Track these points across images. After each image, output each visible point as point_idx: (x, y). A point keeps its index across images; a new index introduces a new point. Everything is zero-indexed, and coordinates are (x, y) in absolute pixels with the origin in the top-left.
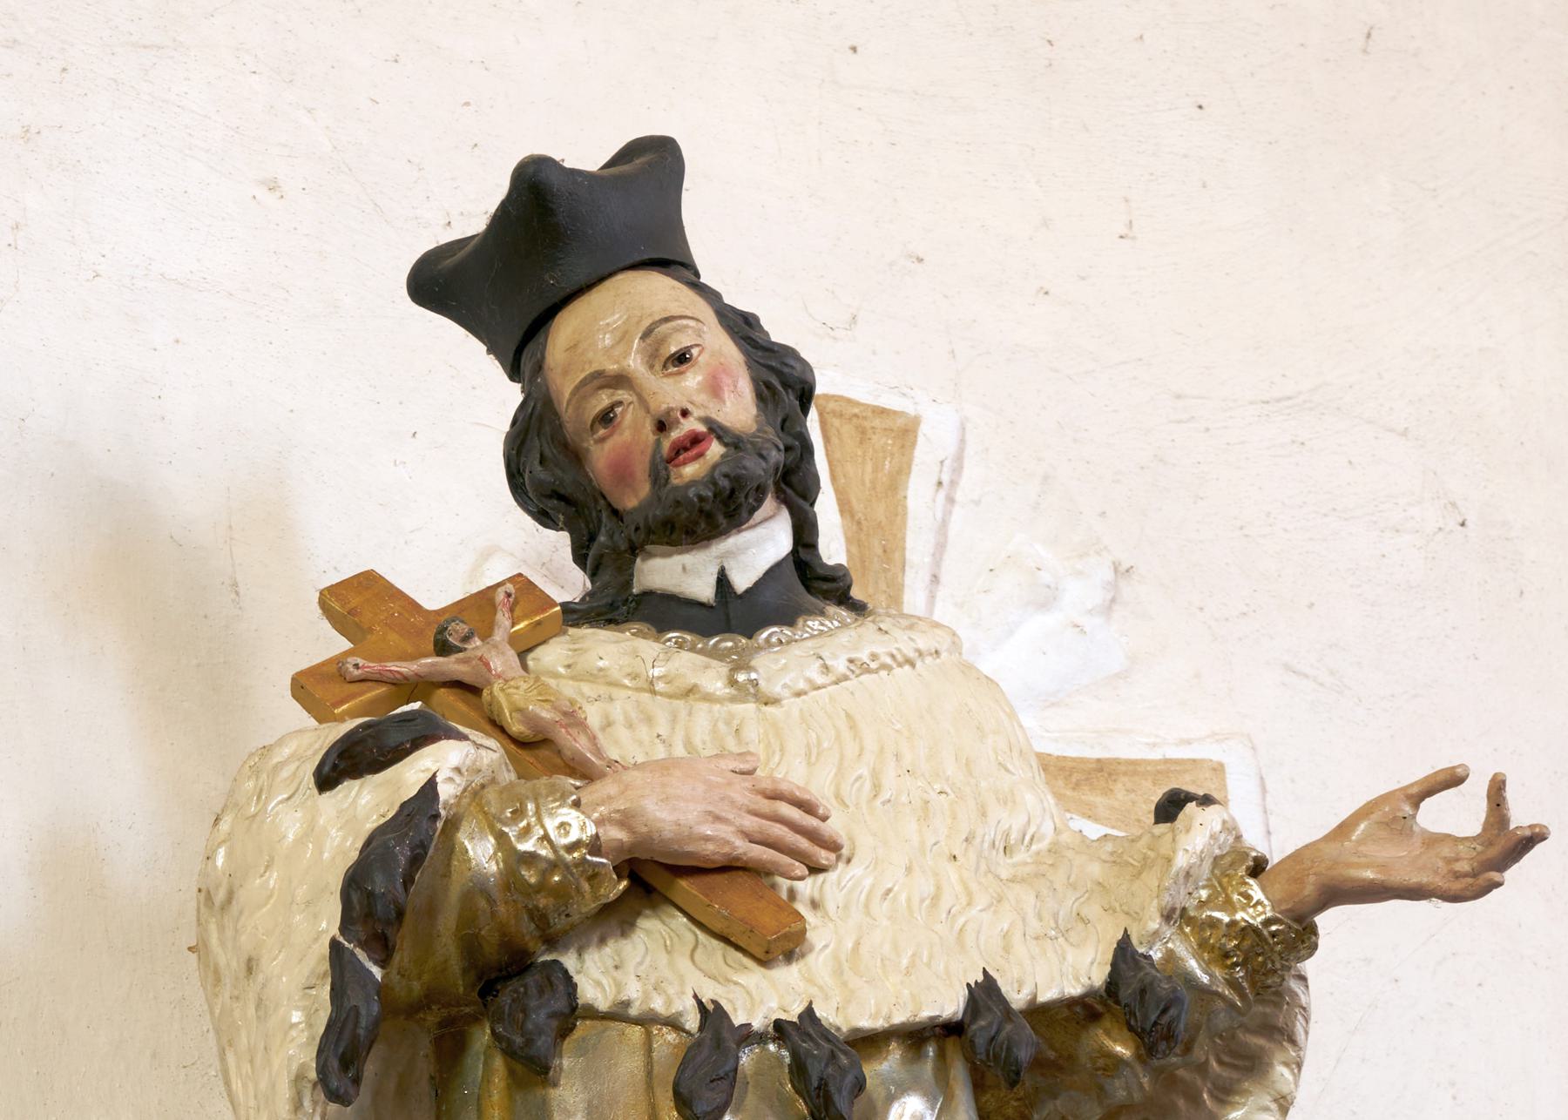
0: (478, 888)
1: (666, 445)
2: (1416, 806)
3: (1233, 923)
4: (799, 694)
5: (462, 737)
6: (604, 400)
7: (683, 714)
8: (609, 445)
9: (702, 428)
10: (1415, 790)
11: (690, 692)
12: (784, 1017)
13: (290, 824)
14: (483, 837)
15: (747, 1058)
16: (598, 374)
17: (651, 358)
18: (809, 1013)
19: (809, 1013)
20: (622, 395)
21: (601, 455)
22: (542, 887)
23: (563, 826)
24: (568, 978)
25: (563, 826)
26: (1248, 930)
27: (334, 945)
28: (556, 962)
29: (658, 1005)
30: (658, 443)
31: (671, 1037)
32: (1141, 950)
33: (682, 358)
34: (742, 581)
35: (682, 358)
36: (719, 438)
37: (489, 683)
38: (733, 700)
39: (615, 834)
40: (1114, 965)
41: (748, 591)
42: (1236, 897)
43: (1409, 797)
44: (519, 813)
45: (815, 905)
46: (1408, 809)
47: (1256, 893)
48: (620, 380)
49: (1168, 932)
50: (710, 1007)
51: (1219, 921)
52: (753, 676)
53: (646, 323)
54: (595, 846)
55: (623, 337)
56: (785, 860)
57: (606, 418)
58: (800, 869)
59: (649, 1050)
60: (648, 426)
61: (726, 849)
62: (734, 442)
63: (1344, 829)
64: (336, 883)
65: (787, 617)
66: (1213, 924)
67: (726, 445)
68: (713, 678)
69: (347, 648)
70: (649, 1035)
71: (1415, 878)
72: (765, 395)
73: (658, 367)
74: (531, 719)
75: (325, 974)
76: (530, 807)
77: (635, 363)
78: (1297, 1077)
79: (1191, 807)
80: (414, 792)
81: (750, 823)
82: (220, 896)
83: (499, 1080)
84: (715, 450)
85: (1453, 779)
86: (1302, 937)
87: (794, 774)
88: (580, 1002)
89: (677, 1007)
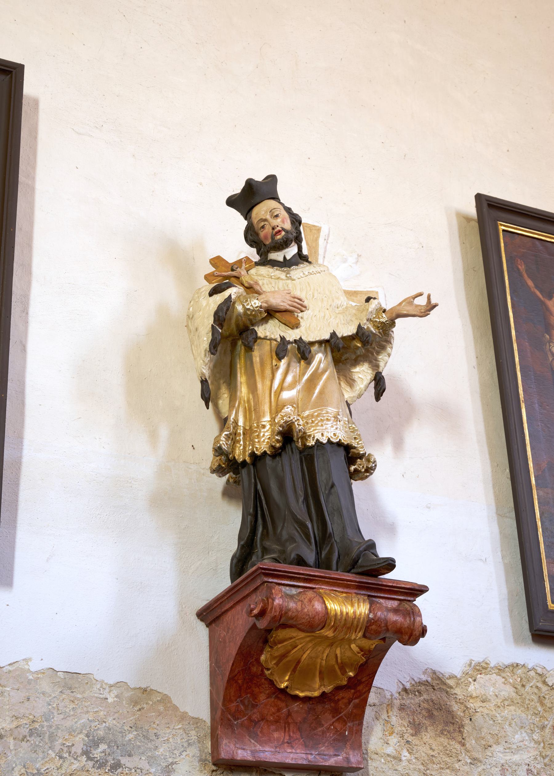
0: (239, 315)
1: (274, 232)
2: (414, 299)
3: (380, 321)
5: (236, 287)
6: (262, 224)
7: (277, 282)
9: (281, 229)
10: (414, 297)
12: (296, 339)
13: (204, 303)
14: (240, 305)
15: (289, 347)
17: (271, 216)
18: (301, 338)
19: (301, 338)
20: (266, 223)
21: (262, 234)
22: (251, 315)
27: (212, 325)
29: (273, 337)
31: (275, 342)
33: (277, 216)
34: (288, 258)
35: (277, 216)
36: (284, 231)
39: (265, 305)
42: (380, 316)
43: (413, 298)
44: (247, 301)
45: (302, 318)
46: (412, 300)
48: (266, 220)
50: (282, 337)
52: (290, 275)
54: (261, 307)
55: (266, 212)
56: (296, 309)
57: (263, 227)
58: (299, 311)
59: (271, 345)
60: (271, 229)
61: (285, 308)
62: (287, 232)
63: (400, 304)
64: (213, 314)
66: (376, 321)
67: (285, 232)
68: (283, 276)
70: (271, 342)
71: (414, 313)
72: (293, 223)
73: (273, 218)
76: (249, 300)
77: (268, 217)
78: (392, 350)
79: (372, 300)
81: (290, 303)
82: (191, 316)
84: (283, 233)
87: (298, 294)
88: (258, 336)
89: (276, 337)
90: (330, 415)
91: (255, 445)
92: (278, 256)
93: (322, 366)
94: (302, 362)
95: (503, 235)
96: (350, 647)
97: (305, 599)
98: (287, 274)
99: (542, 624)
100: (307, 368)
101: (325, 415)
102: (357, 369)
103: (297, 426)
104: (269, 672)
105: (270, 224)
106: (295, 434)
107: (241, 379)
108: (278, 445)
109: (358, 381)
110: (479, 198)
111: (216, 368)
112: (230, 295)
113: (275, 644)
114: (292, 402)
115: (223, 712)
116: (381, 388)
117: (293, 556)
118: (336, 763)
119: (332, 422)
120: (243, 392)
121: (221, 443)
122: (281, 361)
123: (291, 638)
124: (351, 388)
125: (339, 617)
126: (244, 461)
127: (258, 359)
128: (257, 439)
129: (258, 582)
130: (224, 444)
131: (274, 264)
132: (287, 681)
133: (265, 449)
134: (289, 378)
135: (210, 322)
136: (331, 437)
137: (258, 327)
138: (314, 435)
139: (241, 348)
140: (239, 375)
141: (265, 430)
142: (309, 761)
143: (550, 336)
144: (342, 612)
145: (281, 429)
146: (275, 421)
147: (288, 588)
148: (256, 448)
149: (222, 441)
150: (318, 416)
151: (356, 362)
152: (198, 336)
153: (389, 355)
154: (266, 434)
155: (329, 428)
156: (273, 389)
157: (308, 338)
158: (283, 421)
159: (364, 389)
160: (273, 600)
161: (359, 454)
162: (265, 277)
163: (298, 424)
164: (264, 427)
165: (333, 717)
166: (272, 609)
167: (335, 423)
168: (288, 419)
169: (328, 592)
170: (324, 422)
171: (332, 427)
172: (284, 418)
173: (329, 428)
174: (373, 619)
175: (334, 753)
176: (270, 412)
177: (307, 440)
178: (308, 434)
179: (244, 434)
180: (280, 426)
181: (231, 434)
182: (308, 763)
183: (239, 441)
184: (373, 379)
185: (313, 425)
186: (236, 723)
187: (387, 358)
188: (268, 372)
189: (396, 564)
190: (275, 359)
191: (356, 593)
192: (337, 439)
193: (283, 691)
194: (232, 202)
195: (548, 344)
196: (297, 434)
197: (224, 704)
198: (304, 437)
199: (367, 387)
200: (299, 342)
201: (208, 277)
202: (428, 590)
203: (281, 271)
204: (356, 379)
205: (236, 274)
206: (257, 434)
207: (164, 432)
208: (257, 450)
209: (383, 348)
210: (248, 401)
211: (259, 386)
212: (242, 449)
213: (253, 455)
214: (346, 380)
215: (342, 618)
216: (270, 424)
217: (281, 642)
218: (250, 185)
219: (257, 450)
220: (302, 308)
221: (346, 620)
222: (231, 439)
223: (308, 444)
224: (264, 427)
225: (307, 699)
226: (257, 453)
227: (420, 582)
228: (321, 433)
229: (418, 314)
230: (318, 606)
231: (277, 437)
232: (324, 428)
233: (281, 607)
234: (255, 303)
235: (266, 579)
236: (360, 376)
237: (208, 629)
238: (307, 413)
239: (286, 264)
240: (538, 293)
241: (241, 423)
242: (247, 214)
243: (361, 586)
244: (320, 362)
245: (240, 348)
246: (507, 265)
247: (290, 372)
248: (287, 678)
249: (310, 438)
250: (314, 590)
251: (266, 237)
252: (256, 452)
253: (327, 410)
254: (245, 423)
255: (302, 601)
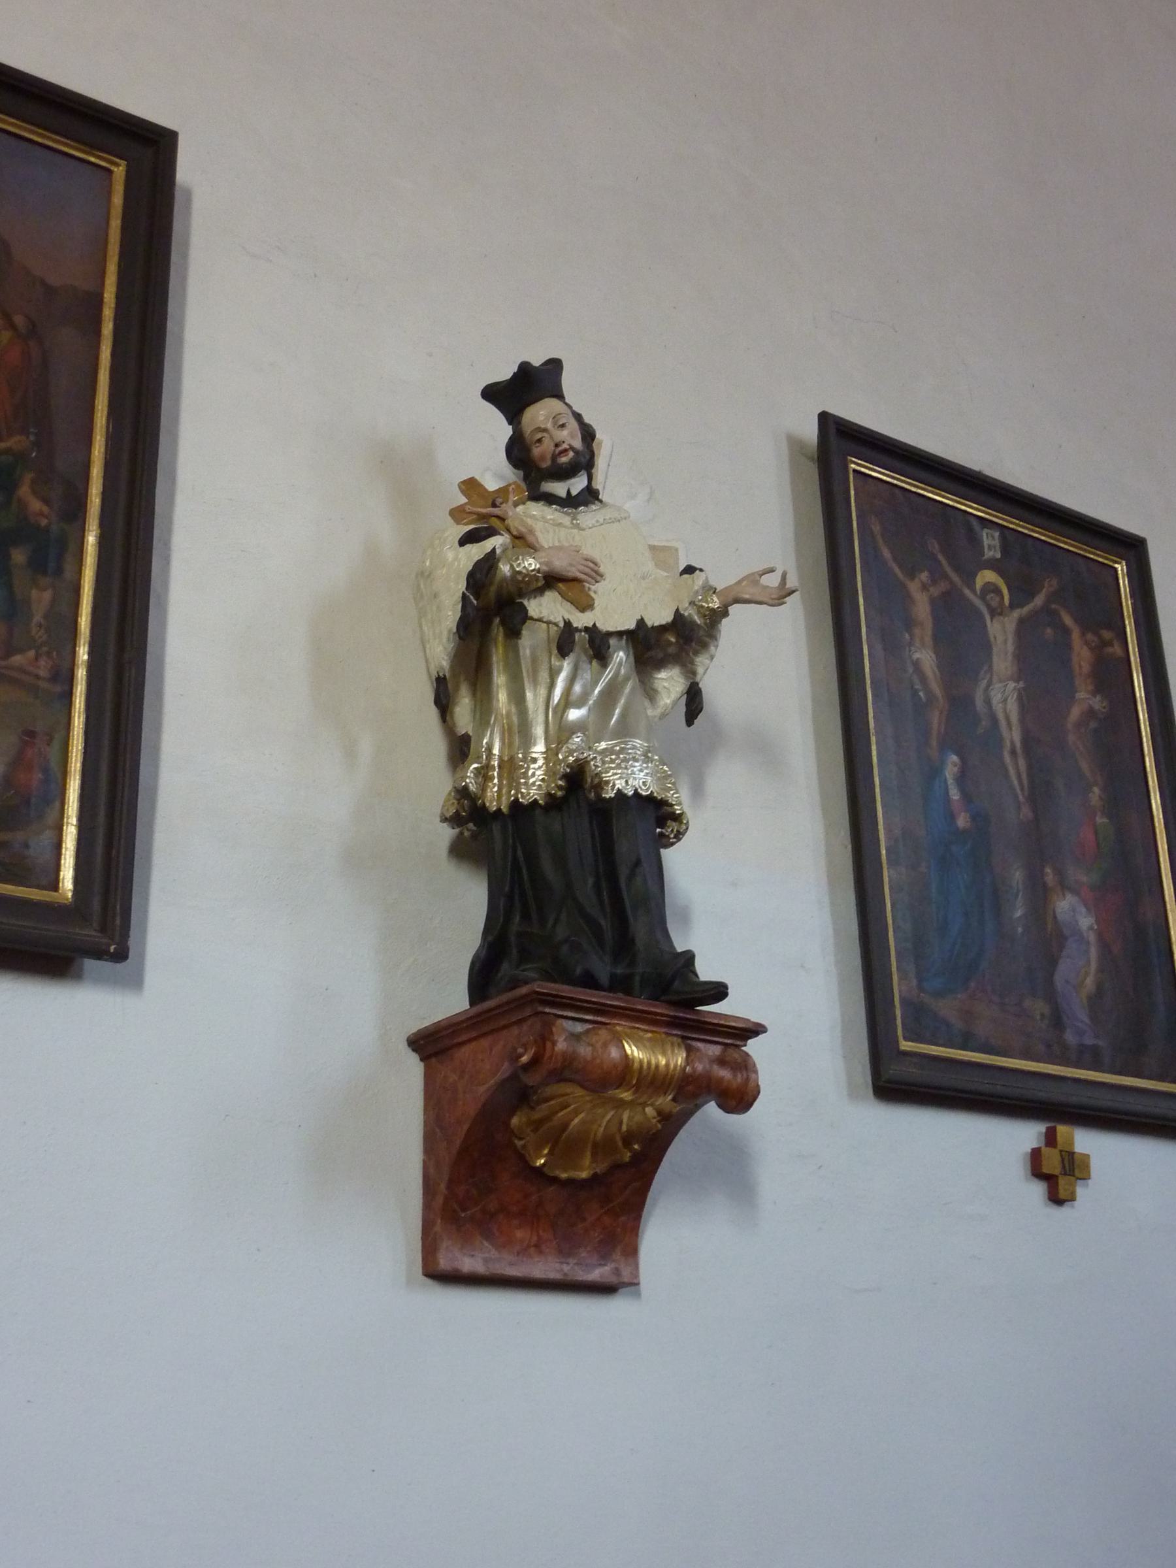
0: (504, 579)
1: (557, 452)
2: (761, 577)
3: (708, 607)
4: (590, 528)
5: (502, 535)
6: (539, 436)
7: (557, 530)
8: (539, 449)
9: (568, 447)
10: (761, 573)
11: (560, 525)
12: (587, 625)
13: (450, 556)
14: (507, 565)
15: (577, 636)
16: (539, 428)
17: (555, 423)
18: (594, 625)
19: (594, 625)
20: (545, 434)
21: (536, 451)
22: (523, 581)
23: (530, 564)
24: (525, 608)
25: (530, 564)
26: (713, 610)
27: (464, 594)
28: (521, 602)
29: (552, 618)
30: (554, 451)
31: (555, 628)
32: (682, 612)
33: (563, 426)
34: (574, 493)
35: (563, 426)
36: (573, 451)
37: (507, 519)
38: (572, 528)
39: (545, 568)
40: (675, 615)
41: (575, 496)
42: (709, 599)
43: (759, 575)
44: (517, 559)
45: (595, 592)
46: (758, 578)
47: (715, 599)
48: (545, 430)
49: (690, 608)
50: (567, 620)
51: (704, 606)
52: (578, 522)
53: (553, 416)
54: (539, 571)
55: (547, 419)
56: (590, 579)
57: (539, 441)
58: (593, 581)
59: (549, 631)
60: (552, 445)
61: (574, 575)
62: (576, 452)
63: (739, 582)
64: (465, 575)
65: (586, 504)
66: (702, 607)
67: (575, 452)
68: (566, 520)
69: (800, 613)
70: (548, 627)
71: (761, 599)
72: (584, 438)
73: (556, 427)
74: (518, 530)
75: (459, 602)
76: (520, 557)
77: (549, 425)
78: (716, 650)
79: (697, 571)
80: (489, 551)
81: (581, 568)
82: (426, 574)
83: (501, 638)
84: (571, 454)
85: (771, 571)
86: (724, 612)
87: (588, 551)
88: (529, 615)
89: (557, 620)
90: (639, 752)
91: (521, 789)
92: (559, 489)
93: (623, 671)
94: (595, 663)
95: (854, 477)
96: (644, 1110)
97: (597, 1042)
98: (573, 519)
99: (895, 1070)
100: (601, 674)
101: (630, 751)
102: (663, 675)
103: (593, 768)
104: (522, 1142)
105: (551, 437)
106: (589, 780)
107: (500, 680)
108: (560, 793)
109: (663, 693)
110: (824, 418)
111: (458, 658)
112: (494, 549)
113: (539, 1103)
114: (580, 726)
115: (447, 1199)
116: (697, 707)
117: (579, 971)
118: (601, 1277)
119: (640, 763)
120: (501, 701)
121: (468, 781)
122: (564, 659)
123: (563, 1095)
124: (652, 703)
125: (645, 1073)
126: (499, 810)
127: (528, 652)
128: (523, 778)
129: (528, 1012)
130: (471, 782)
131: (550, 499)
132: (546, 1155)
133: (536, 796)
134: (577, 688)
135: (460, 587)
136: (640, 787)
137: (528, 600)
138: (614, 783)
139: (498, 629)
140: (495, 673)
141: (536, 766)
142: (565, 1274)
143: (910, 636)
144: (649, 1063)
145: (568, 770)
146: (558, 756)
147: (570, 1022)
148: (522, 793)
149: (469, 777)
150: (622, 750)
151: (660, 664)
152: (438, 607)
153: (712, 658)
154: (538, 773)
155: (637, 773)
156: (551, 702)
157: (605, 626)
158: (574, 759)
159: (670, 706)
160: (554, 1043)
161: (674, 813)
162: (538, 520)
163: (594, 765)
164: (535, 760)
165: (602, 1207)
166: (551, 1057)
167: (645, 765)
168: (581, 757)
169: (628, 1031)
170: (630, 762)
171: (641, 771)
172: (575, 755)
173: (637, 773)
174: (691, 1076)
175: (599, 1263)
176: (546, 739)
177: (603, 789)
178: (604, 779)
179: (500, 767)
180: (567, 766)
181: (482, 768)
182: (562, 1277)
183: (492, 778)
184: (685, 691)
185: (613, 766)
186: (463, 1215)
187: (707, 661)
188: (544, 675)
189: (729, 991)
190: (556, 655)
191: (667, 1034)
192: (648, 791)
193: (539, 1171)
194: (492, 394)
195: (907, 649)
196: (592, 780)
197: (448, 1188)
198: (600, 785)
199: (675, 703)
200: (592, 631)
201: (457, 514)
202: (766, 1032)
203: (563, 512)
204: (659, 689)
205: (499, 512)
206: (524, 770)
207: (366, 747)
208: (523, 797)
209: (704, 646)
210: (508, 714)
211: (529, 695)
212: (496, 792)
213: (515, 805)
214: (645, 690)
215: (649, 1073)
216: (543, 757)
217: (547, 1100)
218: (525, 370)
219: (523, 797)
220: (597, 576)
221: (654, 1074)
222: (481, 776)
223: (603, 796)
224: (535, 760)
225: (571, 1182)
226: (523, 801)
227: (755, 1018)
228: (625, 780)
229: (765, 600)
230: (614, 1053)
231: (560, 783)
232: (629, 772)
233: (564, 1054)
234: (531, 564)
235: (540, 1009)
236: (666, 684)
237: (422, 1065)
238: (603, 745)
239: (571, 502)
240: (897, 570)
241: (496, 751)
242: (513, 416)
243: (674, 1023)
244: (620, 664)
245: (498, 631)
246: (858, 524)
247: (579, 677)
248: (546, 1152)
249: (608, 786)
250: (608, 1026)
251: (543, 458)
252: (521, 800)
253: (634, 744)
254: (501, 750)
255: (592, 1045)
